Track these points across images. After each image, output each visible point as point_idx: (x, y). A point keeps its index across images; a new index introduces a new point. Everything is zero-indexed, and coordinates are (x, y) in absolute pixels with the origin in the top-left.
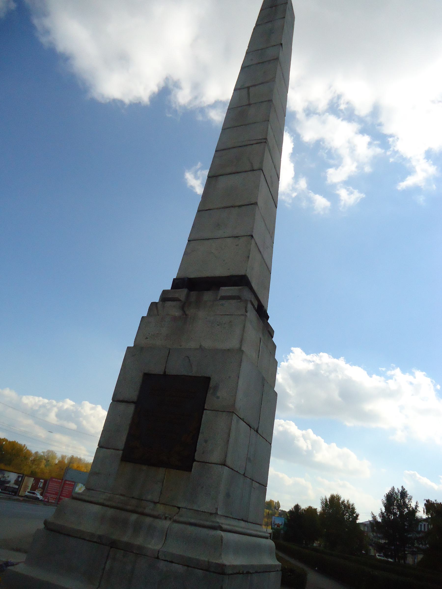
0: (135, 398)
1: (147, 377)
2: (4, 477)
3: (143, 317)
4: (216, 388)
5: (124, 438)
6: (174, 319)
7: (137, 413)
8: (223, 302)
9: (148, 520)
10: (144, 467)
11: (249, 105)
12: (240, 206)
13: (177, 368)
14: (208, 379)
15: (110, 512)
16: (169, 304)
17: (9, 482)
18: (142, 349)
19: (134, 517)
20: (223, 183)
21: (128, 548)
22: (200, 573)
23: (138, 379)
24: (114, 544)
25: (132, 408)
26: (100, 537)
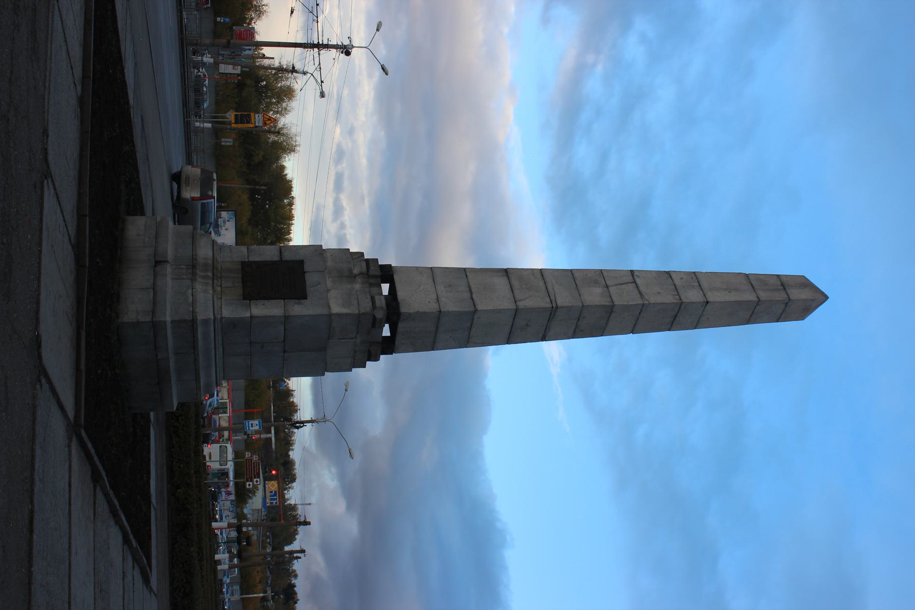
0: (284, 259)
1: (301, 263)
2: (224, 222)
3: (362, 254)
4: (299, 304)
5: (257, 259)
6: (350, 271)
7: (272, 263)
8: (369, 297)
9: (210, 282)
10: (240, 275)
11: (607, 287)
12: (472, 298)
13: (310, 279)
14: (306, 298)
15: (210, 262)
16: (364, 264)
17: (218, 233)
18: (322, 254)
19: (210, 274)
20: (501, 283)
21: (194, 274)
22: (191, 309)
23: (298, 258)
24: (194, 267)
25: (276, 258)
26: (196, 255)
